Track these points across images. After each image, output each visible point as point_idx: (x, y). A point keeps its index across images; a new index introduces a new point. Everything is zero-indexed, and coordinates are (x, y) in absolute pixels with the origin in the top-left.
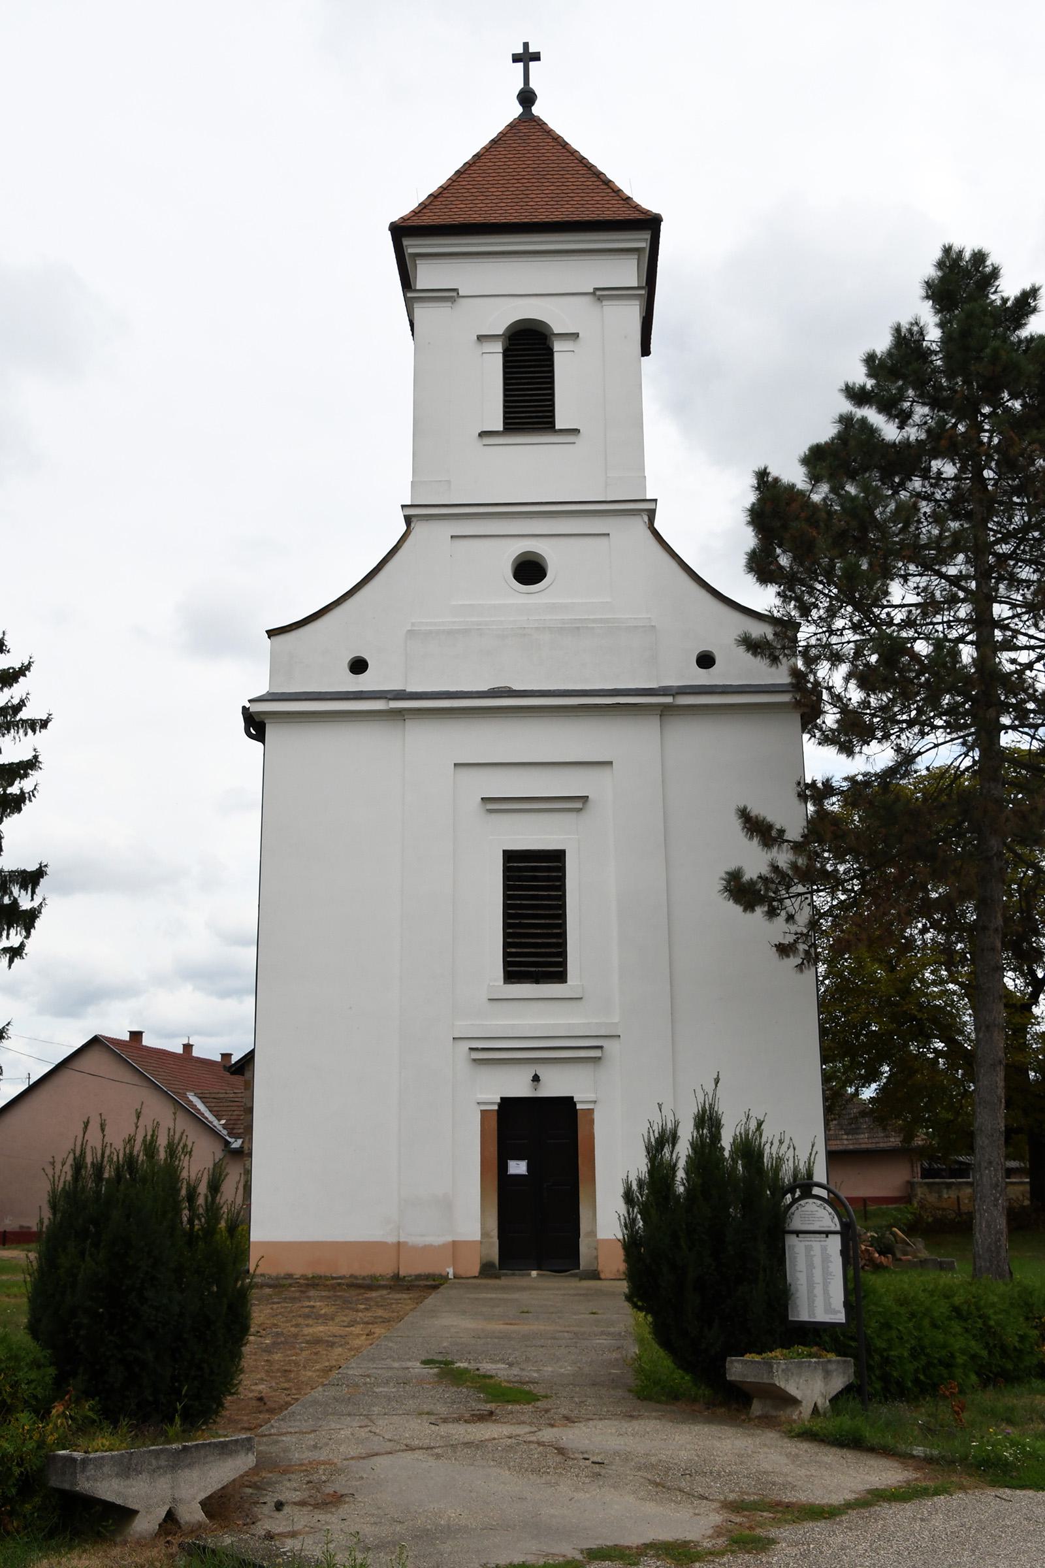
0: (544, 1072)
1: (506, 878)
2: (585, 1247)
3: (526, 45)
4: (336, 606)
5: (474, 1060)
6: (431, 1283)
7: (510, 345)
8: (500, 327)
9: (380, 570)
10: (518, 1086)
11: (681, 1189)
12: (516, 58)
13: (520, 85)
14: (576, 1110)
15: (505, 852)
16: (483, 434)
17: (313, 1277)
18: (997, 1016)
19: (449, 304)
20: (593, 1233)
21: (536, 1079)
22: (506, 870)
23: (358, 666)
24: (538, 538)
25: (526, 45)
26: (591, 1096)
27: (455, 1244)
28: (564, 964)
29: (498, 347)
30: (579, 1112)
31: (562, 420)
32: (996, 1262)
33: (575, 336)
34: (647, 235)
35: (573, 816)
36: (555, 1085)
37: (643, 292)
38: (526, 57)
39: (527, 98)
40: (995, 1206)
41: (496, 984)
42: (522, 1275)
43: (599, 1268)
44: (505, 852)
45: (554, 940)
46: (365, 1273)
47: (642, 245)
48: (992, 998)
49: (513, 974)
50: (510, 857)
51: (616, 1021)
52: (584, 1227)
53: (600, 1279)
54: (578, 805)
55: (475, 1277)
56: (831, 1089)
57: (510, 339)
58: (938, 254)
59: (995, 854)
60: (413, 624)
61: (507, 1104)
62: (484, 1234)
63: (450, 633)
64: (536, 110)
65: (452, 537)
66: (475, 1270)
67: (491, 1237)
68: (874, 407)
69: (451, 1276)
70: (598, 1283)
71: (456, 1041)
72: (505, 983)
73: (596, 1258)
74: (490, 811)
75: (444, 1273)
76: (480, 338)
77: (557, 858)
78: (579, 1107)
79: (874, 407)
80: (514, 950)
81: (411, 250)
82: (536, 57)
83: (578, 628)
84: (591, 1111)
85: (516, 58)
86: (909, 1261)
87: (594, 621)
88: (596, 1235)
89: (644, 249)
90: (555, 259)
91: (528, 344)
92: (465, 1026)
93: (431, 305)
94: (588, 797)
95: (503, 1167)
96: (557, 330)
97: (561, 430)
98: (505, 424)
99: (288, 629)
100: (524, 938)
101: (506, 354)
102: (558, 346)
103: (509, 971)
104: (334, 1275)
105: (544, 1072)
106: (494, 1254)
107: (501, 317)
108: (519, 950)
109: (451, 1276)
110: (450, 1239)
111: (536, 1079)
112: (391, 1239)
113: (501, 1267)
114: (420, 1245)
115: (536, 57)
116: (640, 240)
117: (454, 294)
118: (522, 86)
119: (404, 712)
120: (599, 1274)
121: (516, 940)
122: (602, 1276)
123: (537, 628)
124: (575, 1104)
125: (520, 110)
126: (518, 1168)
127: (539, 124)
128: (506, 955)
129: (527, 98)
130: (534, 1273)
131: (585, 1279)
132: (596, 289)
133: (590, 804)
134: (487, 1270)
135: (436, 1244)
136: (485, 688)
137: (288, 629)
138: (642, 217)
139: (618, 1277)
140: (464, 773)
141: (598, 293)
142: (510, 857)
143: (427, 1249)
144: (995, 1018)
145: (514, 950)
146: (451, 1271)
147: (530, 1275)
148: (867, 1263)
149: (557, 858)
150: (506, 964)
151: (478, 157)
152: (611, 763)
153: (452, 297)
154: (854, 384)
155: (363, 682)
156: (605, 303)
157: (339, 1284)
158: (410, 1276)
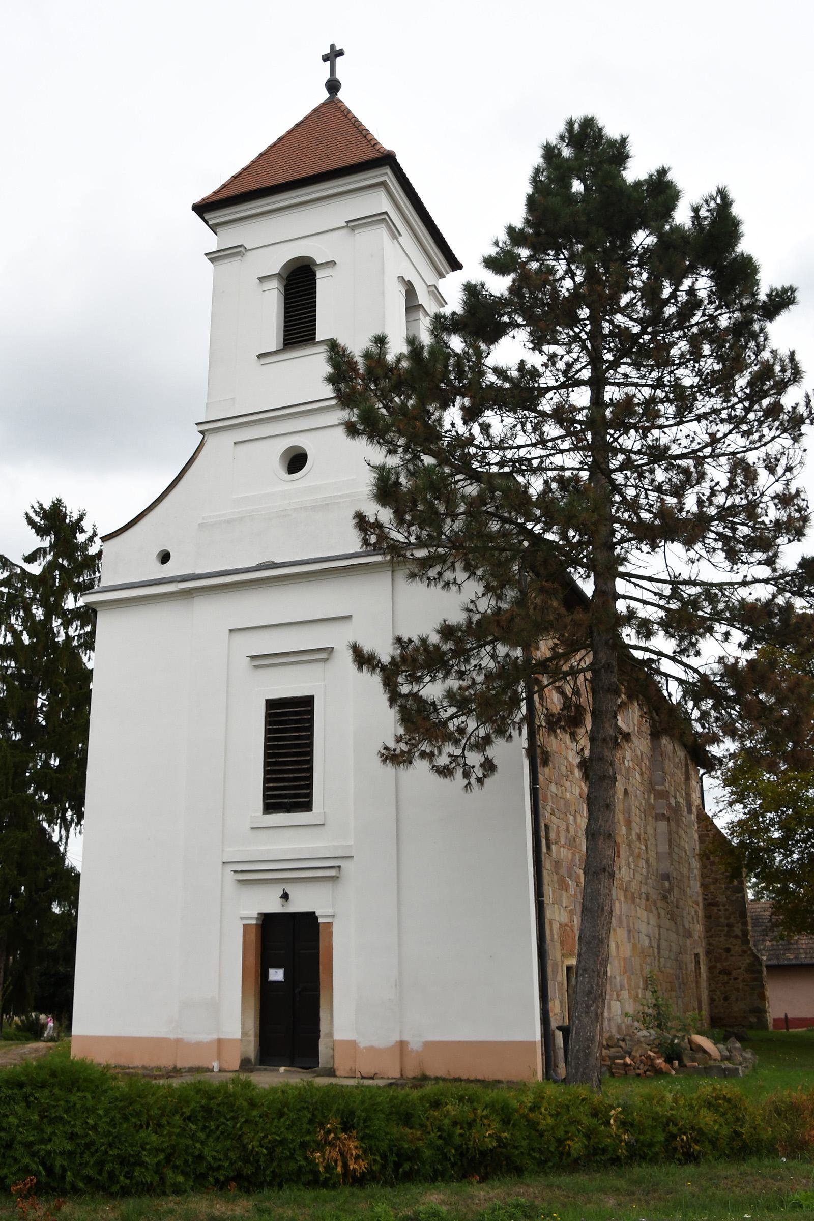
0: (291, 890)
1: (268, 722)
3: (333, 46)
4: (149, 512)
5: (239, 881)
9: (181, 478)
10: (274, 906)
12: (325, 58)
13: (328, 76)
14: (319, 924)
15: (267, 701)
17: (115, 1067)
18: (603, 824)
19: (239, 258)
20: (330, 1035)
21: (285, 896)
22: (268, 716)
23: (165, 557)
24: (302, 434)
25: (333, 46)
26: (330, 911)
27: (220, 1041)
28: (310, 795)
29: (275, 284)
30: (321, 925)
32: (581, 1070)
33: (332, 263)
35: (320, 666)
36: (300, 903)
38: (333, 55)
39: (333, 86)
40: (587, 1013)
41: (257, 815)
42: (271, 1071)
43: (336, 1066)
44: (267, 701)
45: (303, 775)
46: (153, 1064)
48: (597, 807)
49: (271, 805)
50: (271, 704)
51: (352, 843)
53: (335, 1076)
54: (324, 656)
55: (236, 1071)
59: (603, 667)
60: (203, 518)
61: (268, 921)
62: (244, 1033)
63: (230, 522)
64: (341, 95)
65: (235, 443)
66: (236, 1065)
67: (249, 1036)
69: (216, 1070)
70: (333, 1080)
71: (226, 865)
72: (264, 813)
73: (333, 1057)
74: (257, 667)
75: (210, 1067)
76: (261, 279)
77: (307, 702)
78: (320, 921)
80: (271, 785)
82: (341, 53)
83: (327, 504)
84: (330, 925)
85: (325, 58)
86: (694, 1067)
87: (340, 496)
88: (332, 1036)
90: (314, 206)
91: (302, 278)
92: (235, 852)
94: (333, 648)
95: (264, 974)
97: (319, 342)
99: (115, 534)
100: (280, 774)
103: (267, 803)
104: (130, 1066)
105: (291, 890)
106: (251, 1050)
108: (275, 785)
109: (216, 1070)
110: (215, 1037)
111: (285, 896)
112: (172, 1036)
114: (193, 1042)
115: (341, 53)
117: (241, 249)
118: (329, 77)
119: (192, 591)
120: (334, 1072)
121: (296, 775)
122: (338, 1074)
123: (295, 509)
124: (317, 918)
125: (326, 95)
126: (277, 975)
128: (265, 789)
129: (333, 86)
130: (282, 1069)
131: (323, 1076)
132: (347, 222)
133: (335, 654)
134: (245, 1064)
135: (205, 1041)
136: (253, 564)
137: (115, 534)
139: (351, 1075)
140: (239, 638)
141: (350, 225)
142: (271, 704)
143: (199, 1045)
144: (601, 826)
145: (271, 785)
146: (216, 1066)
147: (278, 1071)
148: (650, 1069)
149: (307, 702)
150: (266, 797)
151: (280, 140)
152: (350, 617)
153: (240, 252)
155: (171, 569)
156: (356, 232)
158: (185, 1068)
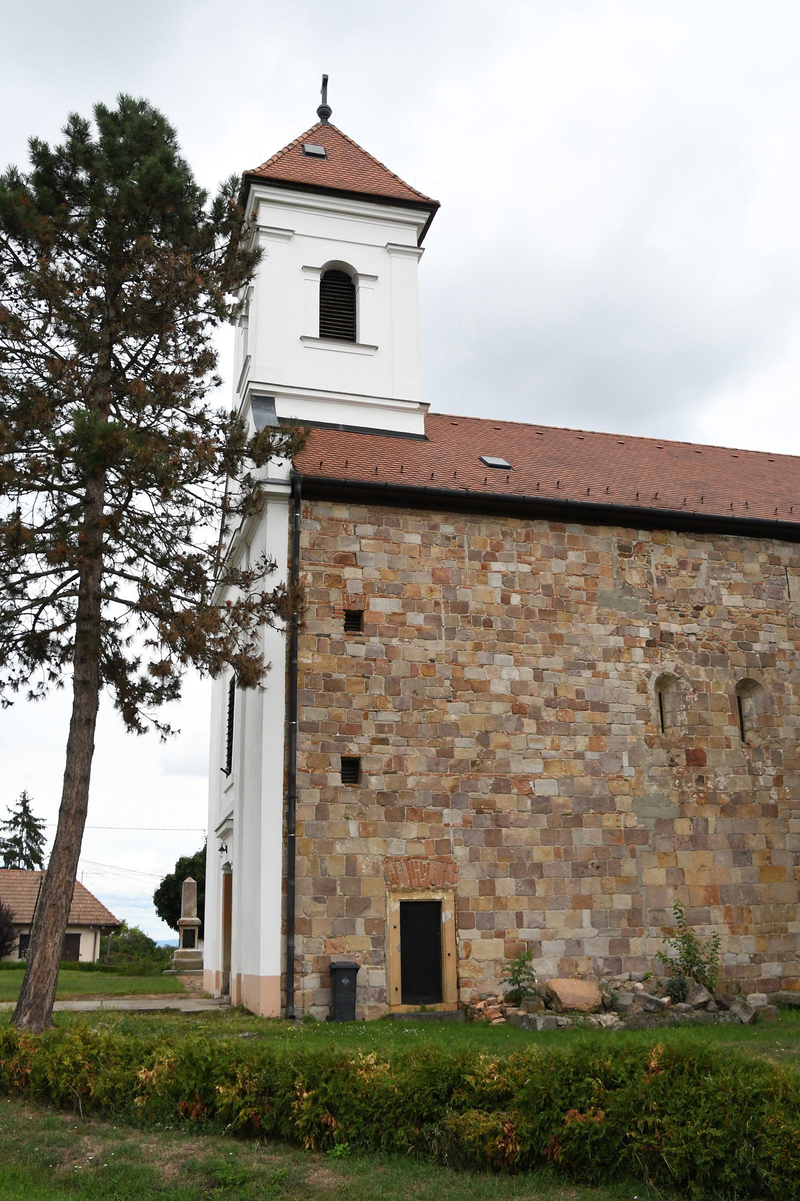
11: (34, 193)
13: (319, 103)
16: (303, 338)
19: (286, 241)
29: (317, 278)
31: (363, 335)
34: (427, 215)
39: (324, 112)
58: (65, 122)
64: (330, 120)
76: (305, 268)
81: (257, 195)
93: (271, 239)
107: (322, 256)
116: (421, 217)
125: (319, 120)
127: (332, 127)
129: (324, 112)
138: (418, 199)
141: (389, 247)
156: (393, 255)
157: (41, 903)
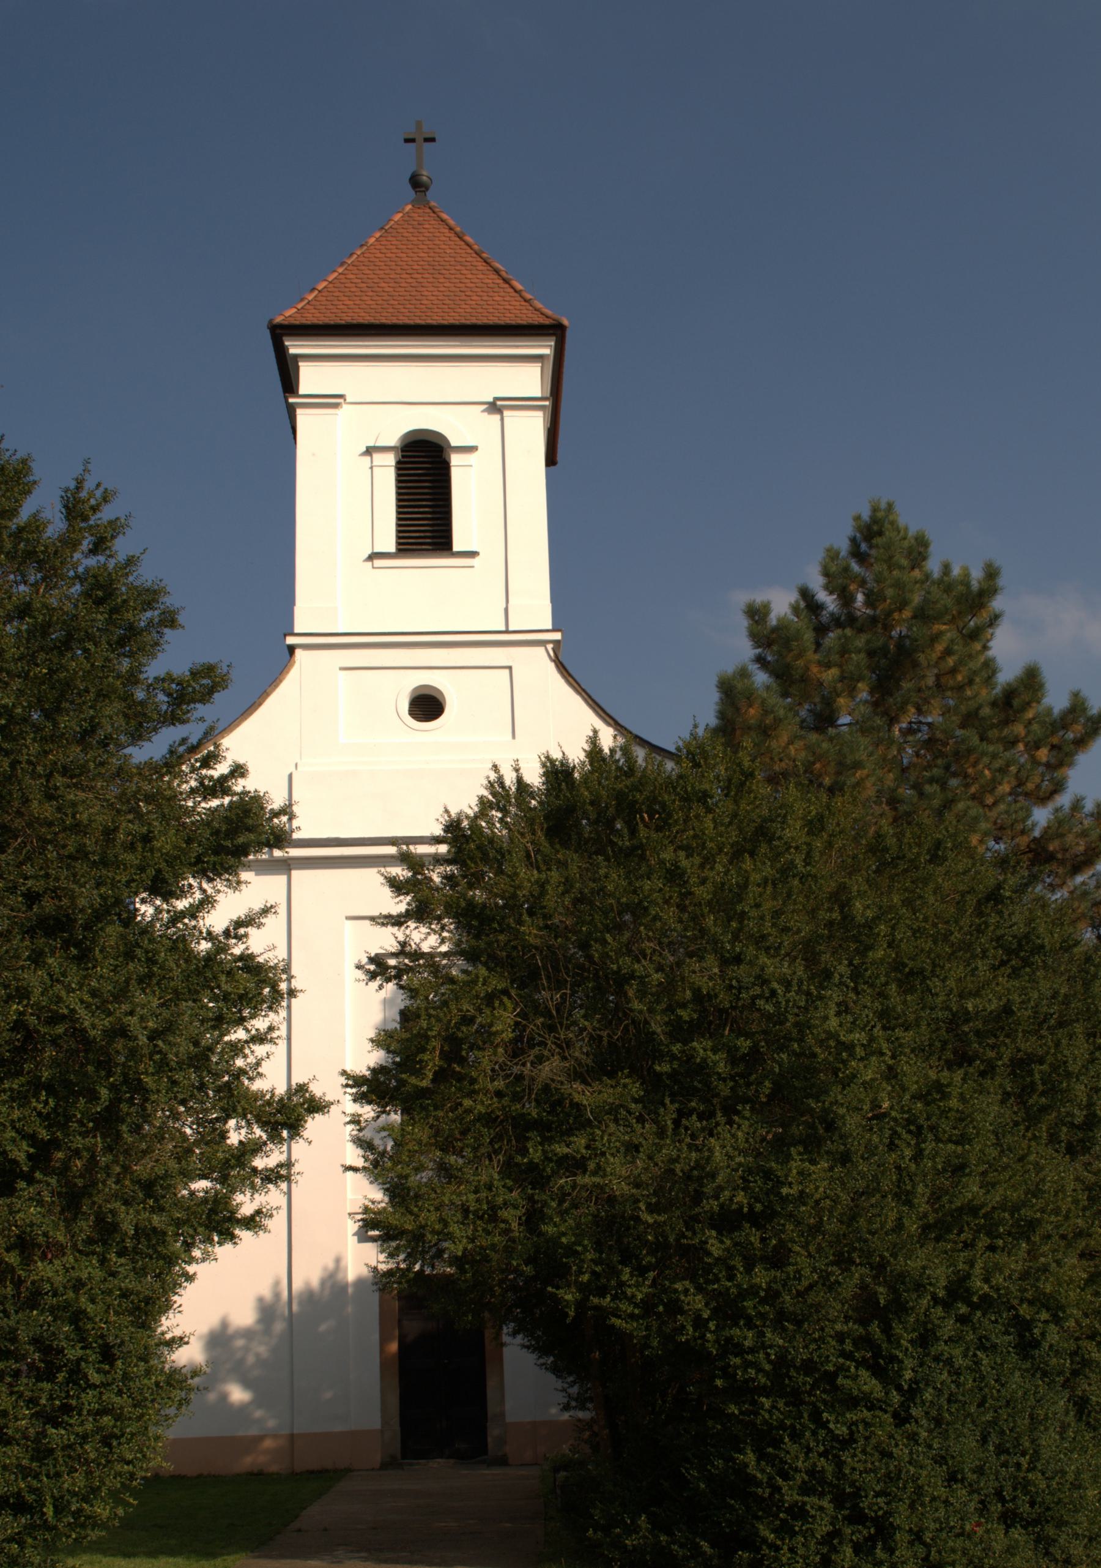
2: (493, 1432)
3: (419, 124)
6: (337, 1474)
7: (403, 457)
8: (393, 438)
25: (419, 124)
33: (470, 449)
37: (547, 403)
47: (547, 351)
52: (492, 1408)
56: (8, 1499)
57: (402, 451)
62: (385, 1422)
68: (367, 1073)
79: (367, 1073)
89: (547, 356)
96: (454, 442)
98: (398, 544)
101: (400, 467)
102: (455, 459)
113: (404, 1457)
132: (496, 399)
141: (499, 403)
154: (313, 1118)
